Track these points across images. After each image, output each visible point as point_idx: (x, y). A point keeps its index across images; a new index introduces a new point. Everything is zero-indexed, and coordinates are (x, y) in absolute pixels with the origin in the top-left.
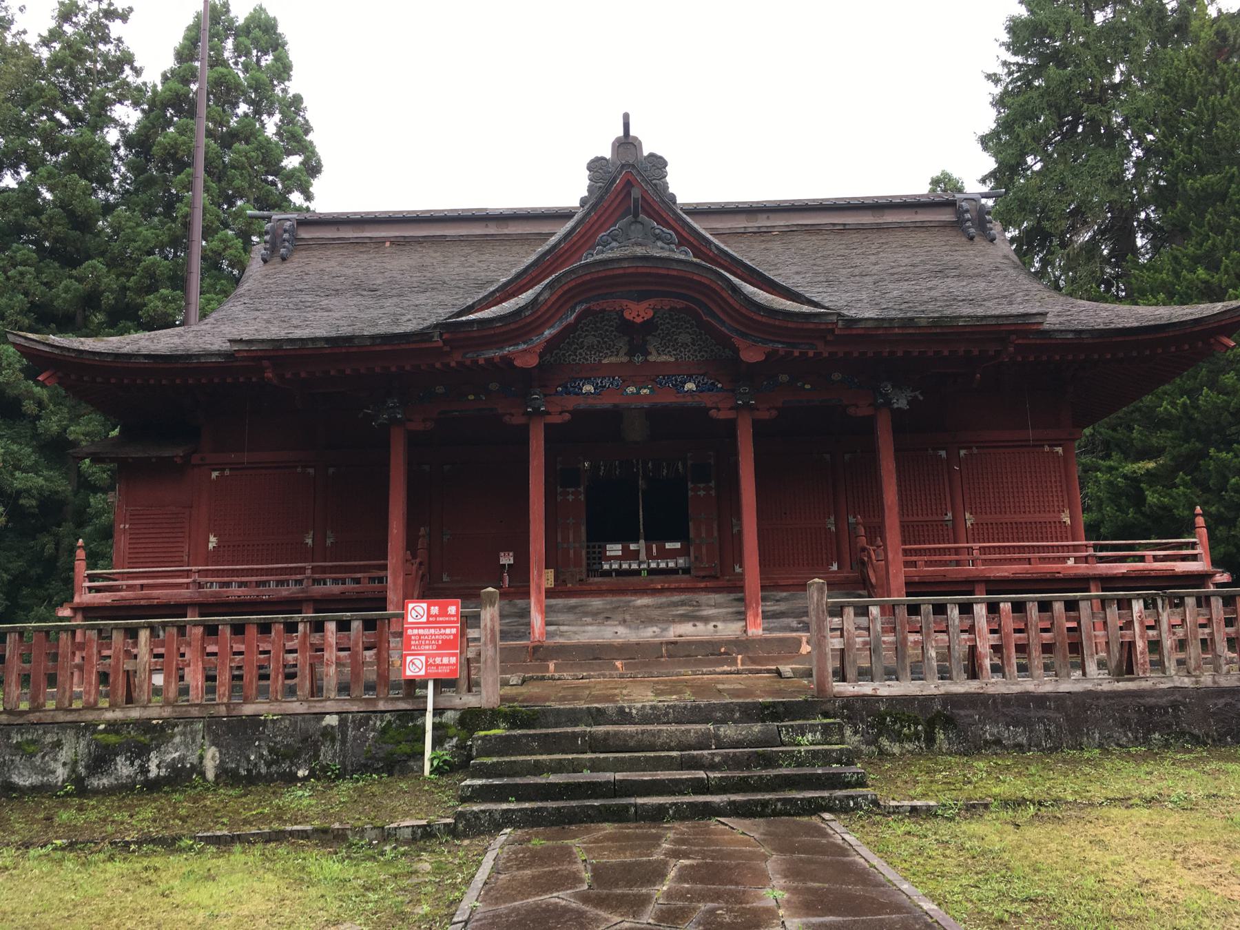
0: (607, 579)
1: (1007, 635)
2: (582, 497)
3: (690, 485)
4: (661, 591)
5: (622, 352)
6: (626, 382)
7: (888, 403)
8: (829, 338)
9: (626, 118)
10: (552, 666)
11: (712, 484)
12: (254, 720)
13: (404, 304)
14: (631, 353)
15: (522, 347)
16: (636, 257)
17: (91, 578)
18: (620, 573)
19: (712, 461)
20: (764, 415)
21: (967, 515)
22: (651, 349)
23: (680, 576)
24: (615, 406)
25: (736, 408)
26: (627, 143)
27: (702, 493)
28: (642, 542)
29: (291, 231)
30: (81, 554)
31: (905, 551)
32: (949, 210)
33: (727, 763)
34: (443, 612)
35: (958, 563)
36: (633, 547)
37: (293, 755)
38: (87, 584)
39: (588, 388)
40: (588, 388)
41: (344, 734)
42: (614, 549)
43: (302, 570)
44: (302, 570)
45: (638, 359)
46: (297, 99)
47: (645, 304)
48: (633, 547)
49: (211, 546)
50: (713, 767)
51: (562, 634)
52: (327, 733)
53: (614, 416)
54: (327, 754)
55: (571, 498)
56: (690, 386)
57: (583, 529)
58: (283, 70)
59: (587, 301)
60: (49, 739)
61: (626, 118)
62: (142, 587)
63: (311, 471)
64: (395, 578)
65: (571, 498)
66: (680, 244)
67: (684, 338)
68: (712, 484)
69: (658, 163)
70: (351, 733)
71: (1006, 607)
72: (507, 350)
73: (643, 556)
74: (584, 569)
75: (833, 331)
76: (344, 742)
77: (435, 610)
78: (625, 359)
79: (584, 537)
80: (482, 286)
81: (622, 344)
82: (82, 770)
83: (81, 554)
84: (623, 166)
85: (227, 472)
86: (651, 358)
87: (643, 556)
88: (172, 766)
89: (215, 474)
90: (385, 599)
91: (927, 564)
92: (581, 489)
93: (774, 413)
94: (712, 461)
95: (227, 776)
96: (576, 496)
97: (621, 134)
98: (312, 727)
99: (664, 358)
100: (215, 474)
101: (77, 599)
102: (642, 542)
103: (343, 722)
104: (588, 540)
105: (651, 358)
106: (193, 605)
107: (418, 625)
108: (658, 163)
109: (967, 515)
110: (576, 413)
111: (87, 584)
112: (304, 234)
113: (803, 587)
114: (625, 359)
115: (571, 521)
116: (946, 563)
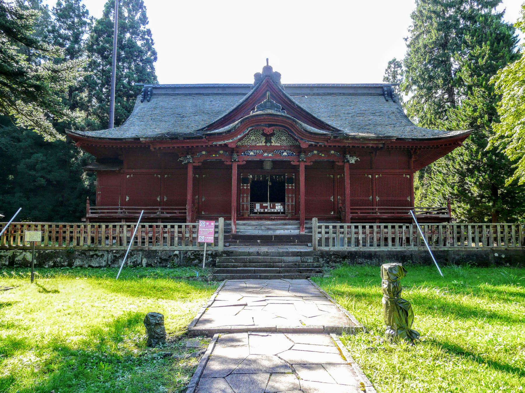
0: (256, 215)
1: (367, 235)
2: (249, 187)
3: (286, 185)
4: (274, 219)
5: (263, 142)
6: (264, 152)
7: (348, 161)
8: (329, 141)
9: (267, 60)
10: (238, 242)
11: (294, 185)
12: (155, 251)
13: (192, 121)
14: (266, 142)
15: (231, 141)
16: (269, 103)
17: (91, 209)
18: (260, 213)
19: (294, 177)
20: (308, 164)
21: (377, 197)
22: (272, 141)
23: (281, 215)
24: (260, 160)
25: (299, 161)
26: (268, 68)
27: (290, 187)
28: (269, 203)
29: (151, 91)
30: (88, 201)
31: (351, 209)
32: (380, 89)
33: (285, 267)
34: (210, 224)
35: (373, 213)
36: (264, 205)
37: (166, 260)
38: (90, 211)
39: (252, 153)
40: (252, 153)
41: (180, 256)
42: (258, 206)
43: (158, 209)
44: (158, 209)
45: (268, 144)
46: (149, 32)
47: (270, 128)
48: (264, 205)
49: (127, 200)
50: (282, 267)
51: (241, 232)
52: (176, 255)
53: (260, 163)
54: (176, 260)
55: (245, 187)
56: (285, 154)
57: (249, 198)
58: (144, 20)
59: (252, 127)
60: (100, 254)
61: (267, 60)
62: (108, 212)
63: (159, 176)
64: (189, 213)
65: (245, 187)
66: (283, 109)
67: (284, 138)
68: (294, 185)
69: (278, 75)
70: (182, 256)
71: (367, 227)
72: (226, 142)
73: (269, 207)
74: (249, 211)
75: (330, 139)
76: (180, 259)
77: (208, 223)
78: (264, 144)
79: (249, 200)
80: (219, 113)
81: (263, 139)
82: (109, 263)
83: (88, 201)
84: (266, 76)
85: (132, 176)
86: (273, 144)
87: (269, 207)
88: (134, 262)
89: (128, 176)
90: (186, 219)
91: (361, 213)
92: (249, 185)
93: (312, 163)
94: (294, 177)
95: (148, 265)
96: (247, 187)
97: (266, 65)
98: (172, 254)
99: (277, 144)
100: (128, 176)
101: (87, 216)
102: (269, 203)
103: (180, 253)
104: (251, 201)
105: (273, 144)
106: (123, 218)
107: (202, 227)
108: (278, 75)
109: (377, 197)
110: (247, 161)
111: (90, 211)
112: (155, 92)
113: (311, 219)
114: (264, 144)
115: (245, 195)
116: (369, 213)
